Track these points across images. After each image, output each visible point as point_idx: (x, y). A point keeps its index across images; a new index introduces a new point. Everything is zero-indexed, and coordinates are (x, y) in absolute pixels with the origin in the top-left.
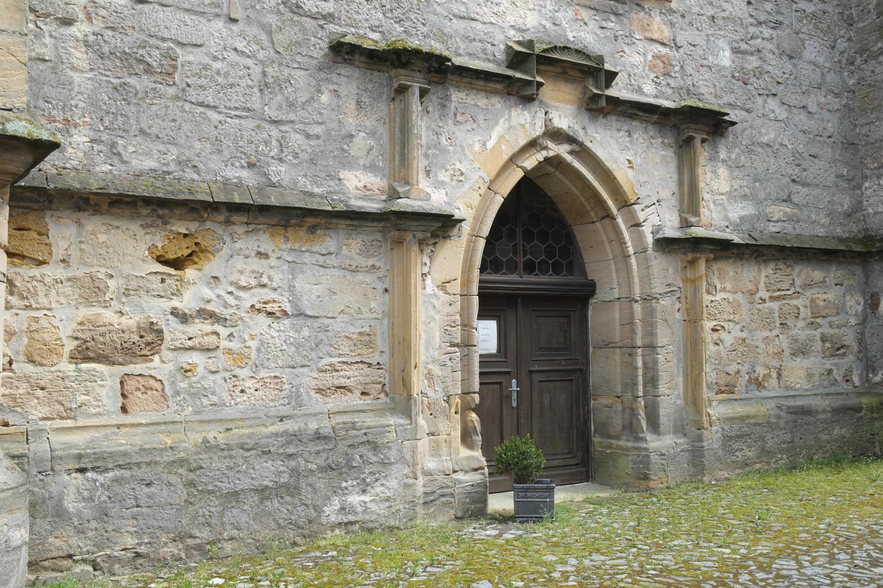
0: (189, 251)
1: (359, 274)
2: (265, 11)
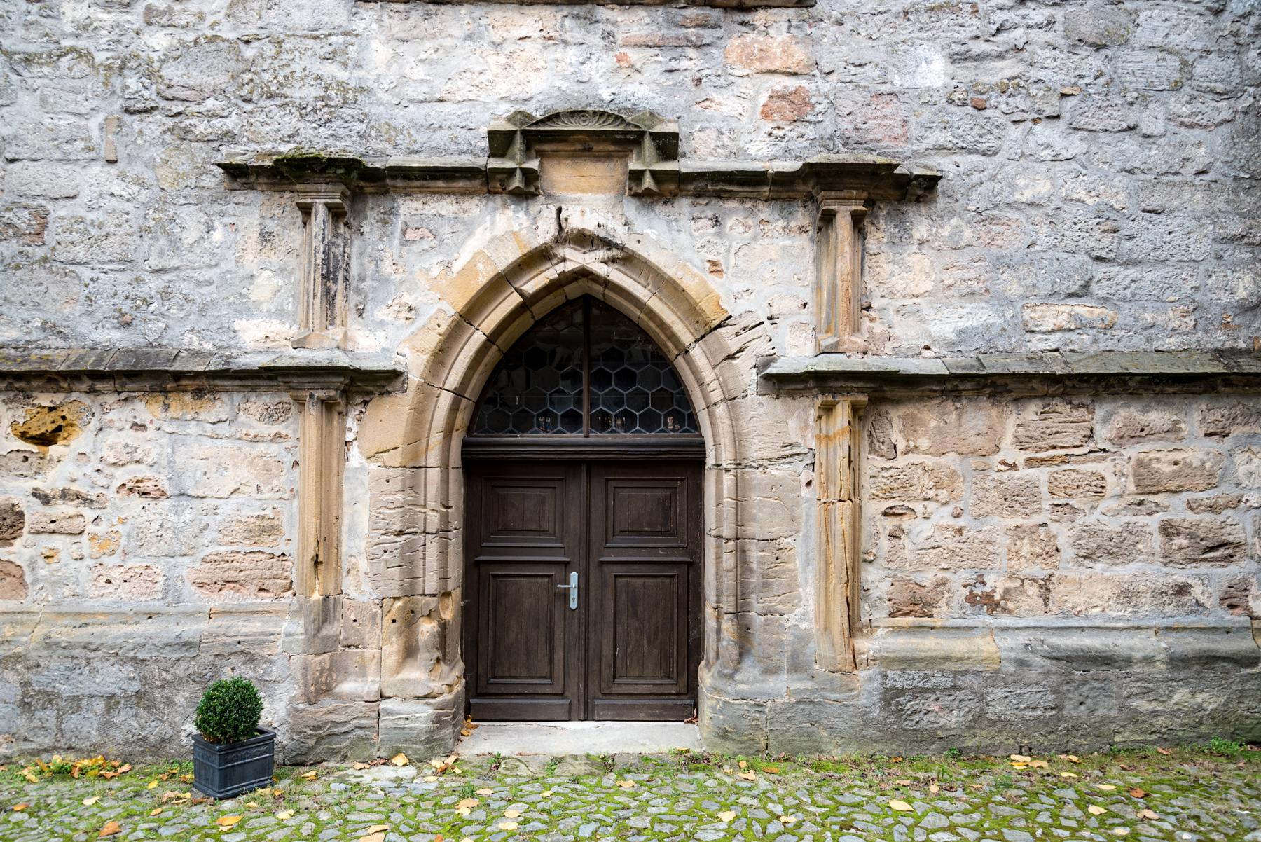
0: (54, 426)
1: (259, 445)
2: (147, 144)
